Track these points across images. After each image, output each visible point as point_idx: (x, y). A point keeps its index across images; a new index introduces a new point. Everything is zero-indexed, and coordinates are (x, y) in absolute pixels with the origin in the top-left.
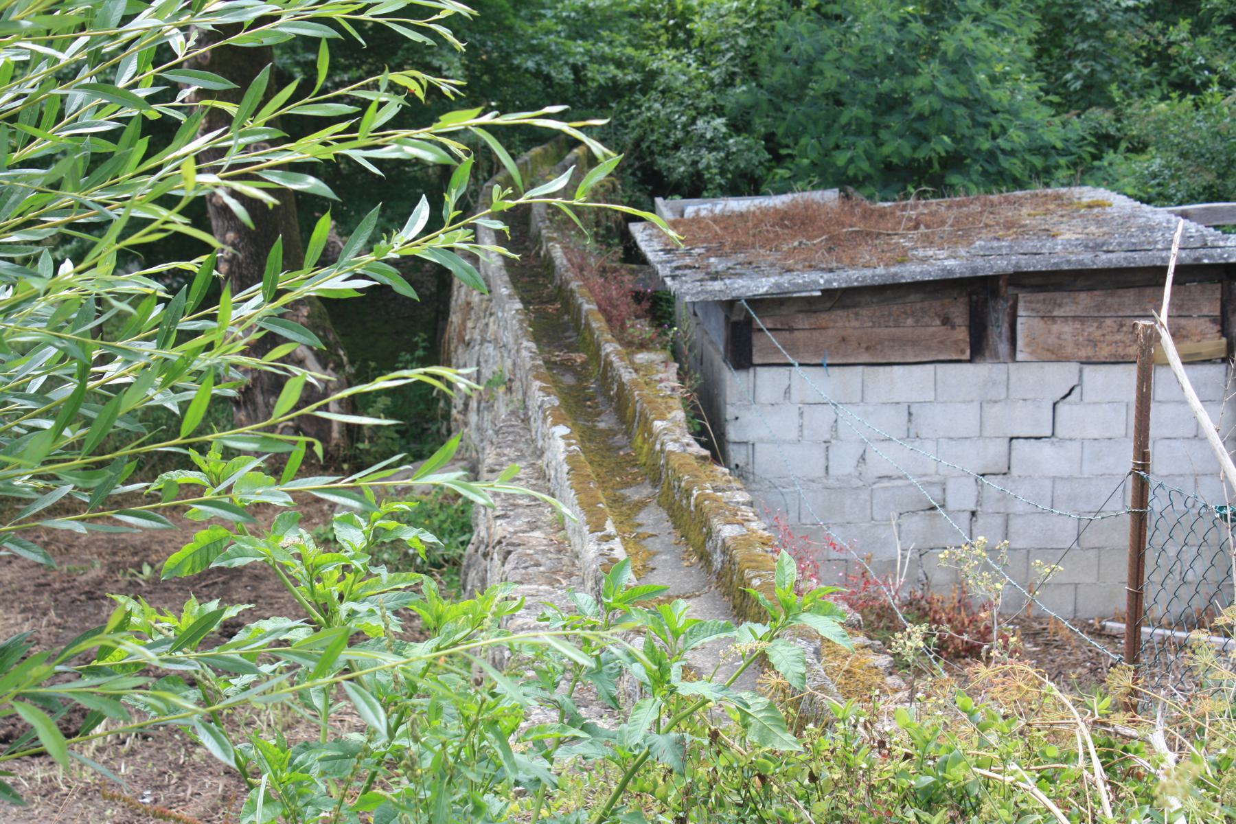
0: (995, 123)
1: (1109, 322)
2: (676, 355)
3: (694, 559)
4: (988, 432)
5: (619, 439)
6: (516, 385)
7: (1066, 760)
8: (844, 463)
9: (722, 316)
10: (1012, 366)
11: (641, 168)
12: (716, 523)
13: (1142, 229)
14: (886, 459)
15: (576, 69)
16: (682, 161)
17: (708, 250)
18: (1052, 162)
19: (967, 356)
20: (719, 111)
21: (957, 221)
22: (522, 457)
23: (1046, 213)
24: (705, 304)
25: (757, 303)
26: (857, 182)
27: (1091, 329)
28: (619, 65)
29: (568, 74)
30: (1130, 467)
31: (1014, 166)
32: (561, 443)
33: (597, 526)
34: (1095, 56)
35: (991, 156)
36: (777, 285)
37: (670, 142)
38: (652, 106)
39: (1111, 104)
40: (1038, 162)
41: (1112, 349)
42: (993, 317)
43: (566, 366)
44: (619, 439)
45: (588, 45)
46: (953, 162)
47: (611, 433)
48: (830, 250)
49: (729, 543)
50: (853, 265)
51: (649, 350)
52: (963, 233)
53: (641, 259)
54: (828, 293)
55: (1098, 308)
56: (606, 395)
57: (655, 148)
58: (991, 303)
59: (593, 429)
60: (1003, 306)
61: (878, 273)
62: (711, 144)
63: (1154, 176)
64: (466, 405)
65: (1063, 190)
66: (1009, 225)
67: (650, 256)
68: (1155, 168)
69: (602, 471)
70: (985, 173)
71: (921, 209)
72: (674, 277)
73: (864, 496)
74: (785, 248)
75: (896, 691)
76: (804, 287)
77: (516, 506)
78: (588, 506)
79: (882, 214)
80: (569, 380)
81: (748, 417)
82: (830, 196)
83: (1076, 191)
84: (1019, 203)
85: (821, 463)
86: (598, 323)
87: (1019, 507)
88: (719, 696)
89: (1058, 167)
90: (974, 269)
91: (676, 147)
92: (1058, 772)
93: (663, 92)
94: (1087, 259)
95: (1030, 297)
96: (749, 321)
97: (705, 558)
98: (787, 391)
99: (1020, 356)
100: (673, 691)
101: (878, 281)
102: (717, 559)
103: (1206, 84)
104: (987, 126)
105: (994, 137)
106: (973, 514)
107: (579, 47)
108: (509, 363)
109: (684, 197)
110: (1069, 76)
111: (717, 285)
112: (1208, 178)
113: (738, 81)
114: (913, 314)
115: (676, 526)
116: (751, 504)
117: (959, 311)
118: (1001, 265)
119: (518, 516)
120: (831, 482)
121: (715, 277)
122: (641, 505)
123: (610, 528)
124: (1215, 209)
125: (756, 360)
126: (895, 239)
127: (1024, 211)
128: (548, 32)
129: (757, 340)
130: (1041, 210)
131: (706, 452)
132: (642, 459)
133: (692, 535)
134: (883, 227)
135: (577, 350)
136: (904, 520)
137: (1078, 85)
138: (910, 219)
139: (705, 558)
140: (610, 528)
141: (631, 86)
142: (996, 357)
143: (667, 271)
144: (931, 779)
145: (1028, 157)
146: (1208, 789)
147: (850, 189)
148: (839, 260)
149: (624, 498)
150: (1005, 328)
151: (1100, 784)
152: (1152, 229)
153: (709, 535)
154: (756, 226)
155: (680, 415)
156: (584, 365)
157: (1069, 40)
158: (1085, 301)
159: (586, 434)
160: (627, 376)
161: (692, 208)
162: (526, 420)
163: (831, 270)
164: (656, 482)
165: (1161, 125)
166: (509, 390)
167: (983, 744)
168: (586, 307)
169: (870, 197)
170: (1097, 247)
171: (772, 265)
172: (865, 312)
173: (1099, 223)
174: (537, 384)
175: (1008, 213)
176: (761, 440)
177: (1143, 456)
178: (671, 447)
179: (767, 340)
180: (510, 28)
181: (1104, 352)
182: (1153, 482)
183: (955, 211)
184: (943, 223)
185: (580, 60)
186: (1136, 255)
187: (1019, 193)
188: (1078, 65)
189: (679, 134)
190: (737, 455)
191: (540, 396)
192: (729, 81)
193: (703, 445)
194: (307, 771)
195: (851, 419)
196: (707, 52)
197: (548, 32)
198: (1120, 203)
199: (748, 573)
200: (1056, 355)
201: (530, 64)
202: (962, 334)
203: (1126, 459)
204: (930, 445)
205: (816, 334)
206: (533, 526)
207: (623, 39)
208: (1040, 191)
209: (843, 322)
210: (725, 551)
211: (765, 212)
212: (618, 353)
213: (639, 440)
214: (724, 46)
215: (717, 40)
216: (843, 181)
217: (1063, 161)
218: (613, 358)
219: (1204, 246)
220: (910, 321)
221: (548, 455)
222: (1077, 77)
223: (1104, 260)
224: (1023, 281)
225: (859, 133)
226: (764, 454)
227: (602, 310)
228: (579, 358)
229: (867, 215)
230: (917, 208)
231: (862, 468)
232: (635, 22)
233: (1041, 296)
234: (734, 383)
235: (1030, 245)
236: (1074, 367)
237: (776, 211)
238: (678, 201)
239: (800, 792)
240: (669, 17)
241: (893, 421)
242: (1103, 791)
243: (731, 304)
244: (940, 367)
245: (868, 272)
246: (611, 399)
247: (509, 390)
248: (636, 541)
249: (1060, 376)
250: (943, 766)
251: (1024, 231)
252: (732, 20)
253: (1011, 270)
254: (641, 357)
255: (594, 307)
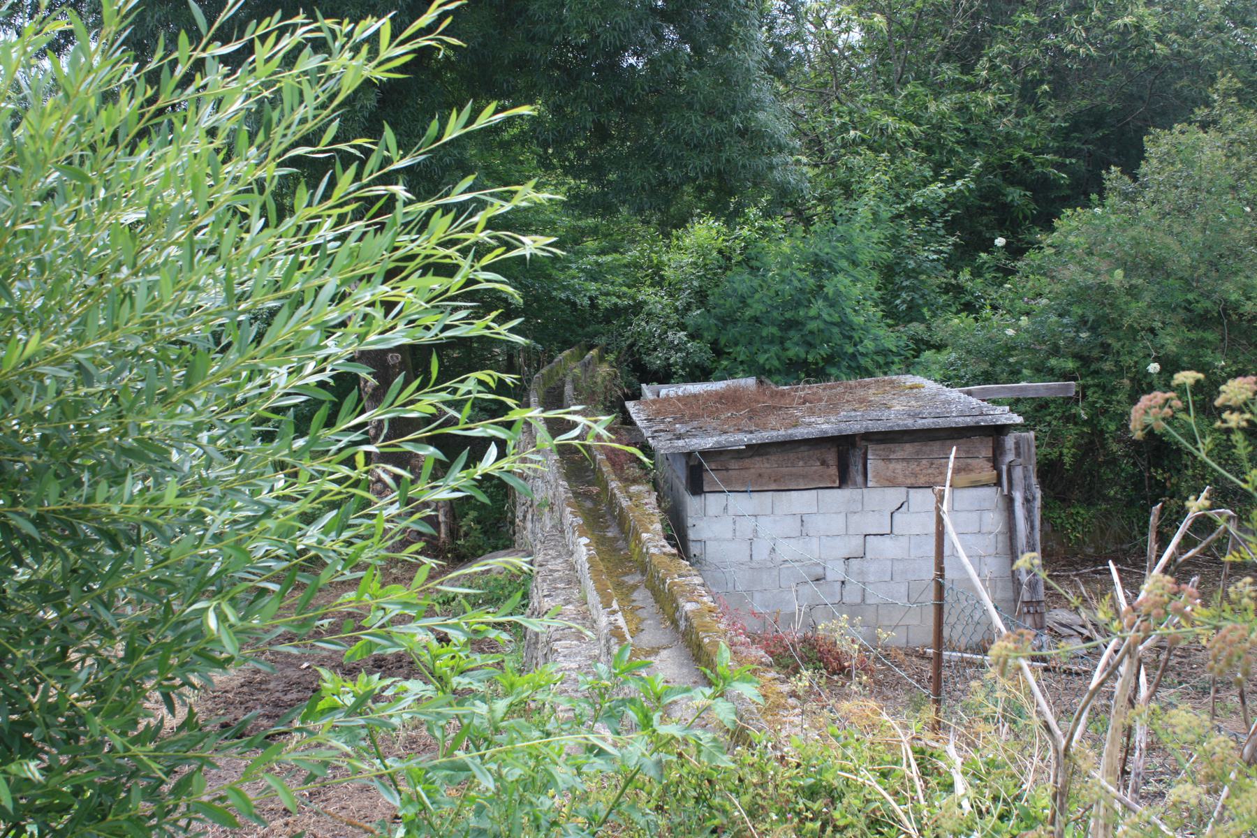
0: (856, 336)
1: (924, 462)
2: (656, 486)
3: (668, 623)
4: (851, 531)
5: (621, 543)
6: (556, 508)
7: (896, 763)
8: (762, 553)
9: (684, 461)
10: (865, 490)
11: (632, 362)
12: (681, 601)
13: (943, 403)
14: (788, 549)
15: (591, 298)
16: (657, 357)
17: (675, 419)
18: (889, 360)
19: (837, 484)
20: (683, 327)
21: (830, 399)
22: (560, 556)
23: (885, 392)
24: (673, 454)
25: (706, 454)
26: (769, 373)
27: (913, 466)
28: (619, 297)
29: (586, 302)
30: (932, 576)
31: (866, 362)
32: (584, 549)
33: (607, 605)
34: (913, 289)
35: (853, 356)
36: (718, 442)
37: (651, 346)
38: (639, 324)
39: (922, 320)
40: (881, 359)
41: (927, 479)
42: (852, 460)
43: (587, 496)
44: (621, 543)
45: (599, 285)
46: (830, 360)
47: (615, 539)
48: (750, 418)
49: (689, 614)
50: (765, 429)
51: (639, 484)
52: (833, 407)
53: (632, 423)
54: (749, 447)
55: (917, 453)
56: (612, 514)
57: (643, 350)
58: (851, 452)
59: (604, 537)
60: (859, 453)
61: (780, 434)
62: (678, 349)
63: (952, 365)
64: (525, 517)
65: (895, 377)
66: (862, 401)
67: (639, 423)
68: (952, 359)
69: (610, 565)
70: (849, 367)
71: (807, 391)
72: (653, 438)
73: (775, 573)
74: (723, 417)
75: (794, 708)
76: (735, 443)
77: (556, 588)
78: (602, 591)
79: (783, 394)
80: (589, 504)
81: (701, 524)
82: (751, 382)
83: (902, 378)
84: (867, 386)
85: (748, 552)
86: (606, 468)
87: (871, 578)
88: (683, 734)
89: (893, 363)
90: (840, 431)
91: (655, 349)
92: (890, 771)
93: (648, 314)
94: (910, 423)
95: (875, 447)
96: (701, 465)
97: (675, 623)
98: (726, 508)
99: (870, 484)
100: (654, 731)
101: (781, 439)
102: (682, 624)
103: (982, 307)
104: (851, 338)
105: (855, 345)
106: (843, 583)
107: (593, 286)
108: (551, 493)
109: (660, 383)
110: (898, 302)
111: (681, 443)
112: (985, 366)
113: (694, 307)
114: (802, 459)
115: (657, 602)
116: (703, 585)
117: (832, 457)
118: (856, 427)
119: (558, 595)
120: (753, 565)
121: (679, 437)
122: (634, 588)
123: (615, 606)
124: (988, 389)
125: (706, 489)
126: (791, 411)
127: (871, 391)
128: (574, 278)
129: (706, 477)
130: (880, 391)
131: (674, 551)
132: (635, 557)
133: (667, 608)
134: (782, 403)
135: (594, 485)
136: (800, 587)
137: (904, 307)
138: (800, 397)
139: (675, 623)
140: (615, 606)
141: (626, 308)
142: (855, 485)
143: (649, 434)
144: (813, 781)
145: (875, 357)
146: (981, 779)
147: (763, 378)
148: (757, 425)
149: (624, 583)
150: (860, 467)
151: (916, 779)
152: (949, 403)
153: (677, 608)
154: (704, 403)
155: (658, 526)
156: (598, 494)
157: (897, 280)
158: (909, 449)
159: (601, 543)
160: (625, 503)
161: (666, 391)
162: (562, 531)
163: (751, 432)
164: (644, 572)
165: (955, 334)
166: (551, 510)
167: (845, 757)
168: (599, 457)
169: (777, 383)
170: (915, 416)
171: (715, 429)
172: (773, 458)
173: (917, 399)
174: (569, 509)
175: (861, 393)
176: (710, 539)
177: (940, 568)
178: (652, 550)
179: (711, 477)
180: (550, 275)
181: (922, 481)
182: (947, 585)
183: (828, 392)
184: (820, 400)
185: (593, 294)
186: (940, 420)
187: (867, 380)
188: (904, 295)
189: (657, 341)
190: (694, 549)
191: (571, 518)
192: (688, 307)
193: (673, 546)
194: (433, 783)
195: (767, 527)
196: (673, 290)
197: (574, 278)
198: (930, 386)
199: (702, 635)
200: (892, 483)
201: (563, 296)
202: (833, 471)
203: (932, 573)
204: (815, 540)
205: (743, 472)
206: (567, 602)
207: (620, 280)
208: (881, 377)
209: (760, 465)
210: (687, 619)
211: (709, 394)
212: (619, 488)
213: (633, 545)
214: (684, 286)
215: (681, 282)
216: (761, 373)
217: (896, 359)
218: (616, 491)
219: (982, 414)
220: (801, 463)
221: (576, 556)
222: (903, 302)
223: (921, 424)
224: (869, 437)
225: (771, 342)
226: (711, 548)
227: (609, 459)
228: (595, 489)
229: (774, 395)
230: (805, 390)
231: (773, 556)
232: (627, 270)
233: (882, 446)
234: (692, 504)
235: (874, 414)
236: (904, 490)
237: (717, 392)
238: (656, 386)
239: (733, 788)
240: (649, 267)
241: (792, 526)
242: (919, 784)
243: (689, 455)
244: (820, 491)
245: (775, 433)
246: (615, 517)
247: (551, 510)
248: (631, 611)
249: (895, 496)
250: (820, 772)
251: (870, 404)
252: (688, 270)
253: (863, 431)
254: (634, 489)
255: (604, 457)
